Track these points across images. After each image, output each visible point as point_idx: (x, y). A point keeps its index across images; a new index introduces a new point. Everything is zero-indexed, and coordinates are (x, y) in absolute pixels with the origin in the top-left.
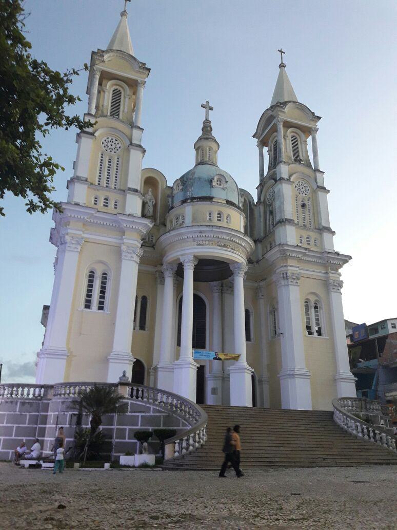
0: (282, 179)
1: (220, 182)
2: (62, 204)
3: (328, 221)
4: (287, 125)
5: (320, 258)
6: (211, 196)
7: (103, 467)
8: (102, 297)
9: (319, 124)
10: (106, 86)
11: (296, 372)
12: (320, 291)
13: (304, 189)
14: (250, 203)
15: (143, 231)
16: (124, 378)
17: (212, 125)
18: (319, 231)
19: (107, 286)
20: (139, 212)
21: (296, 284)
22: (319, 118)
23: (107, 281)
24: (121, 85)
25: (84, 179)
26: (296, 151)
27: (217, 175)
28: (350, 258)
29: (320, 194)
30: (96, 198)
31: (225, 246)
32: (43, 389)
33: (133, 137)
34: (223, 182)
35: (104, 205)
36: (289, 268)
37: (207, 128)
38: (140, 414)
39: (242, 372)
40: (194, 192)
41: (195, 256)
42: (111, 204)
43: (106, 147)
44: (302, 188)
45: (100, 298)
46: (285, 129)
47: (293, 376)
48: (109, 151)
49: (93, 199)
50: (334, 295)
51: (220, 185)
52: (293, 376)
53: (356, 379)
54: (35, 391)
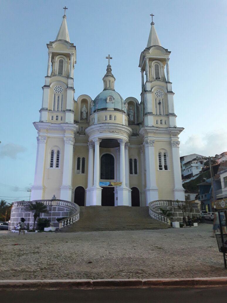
0: (147, 91)
3: (173, 110)
4: (151, 60)
5: (166, 131)
6: (106, 107)
7: (35, 232)
8: (58, 162)
9: (170, 56)
10: (55, 60)
11: (151, 188)
12: (167, 148)
13: (160, 95)
14: (137, 104)
15: (74, 129)
16: (54, 198)
17: (112, 68)
18: (167, 116)
20: (72, 122)
22: (170, 52)
24: (62, 57)
25: (46, 109)
26: (157, 73)
27: (109, 96)
28: (183, 129)
29: (169, 96)
31: (113, 132)
33: (68, 84)
34: (112, 99)
35: (56, 120)
36: (149, 138)
37: (109, 69)
38: (61, 212)
39: (122, 190)
40: (99, 106)
41: (99, 138)
42: (59, 118)
44: (159, 94)
45: (57, 162)
46: (154, 61)
47: (149, 190)
48: (58, 92)
49: (51, 117)
50: (174, 149)
51: (111, 101)
52: (149, 190)
53: (132, 190)
54: (174, 204)
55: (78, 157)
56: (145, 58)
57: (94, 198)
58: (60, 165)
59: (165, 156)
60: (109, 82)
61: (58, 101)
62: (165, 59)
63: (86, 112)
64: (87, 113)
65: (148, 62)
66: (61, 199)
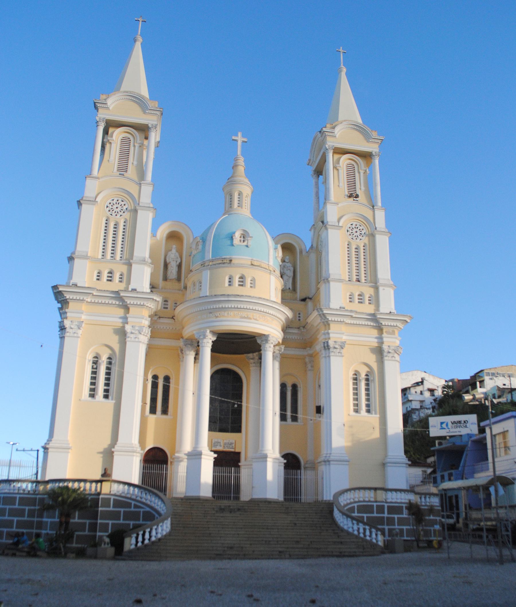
1: (244, 238)
2: (120, 292)
4: (341, 152)
11: (332, 458)
13: (358, 234)
20: (147, 288)
21: (340, 354)
42: (105, 276)
47: (327, 462)
48: (114, 214)
51: (244, 241)
52: (327, 462)
53: (285, 461)
56: (324, 148)
59: (367, 380)
60: (239, 195)
61: (115, 231)
62: (371, 153)
63: (178, 263)
64: (180, 266)
65: (331, 154)
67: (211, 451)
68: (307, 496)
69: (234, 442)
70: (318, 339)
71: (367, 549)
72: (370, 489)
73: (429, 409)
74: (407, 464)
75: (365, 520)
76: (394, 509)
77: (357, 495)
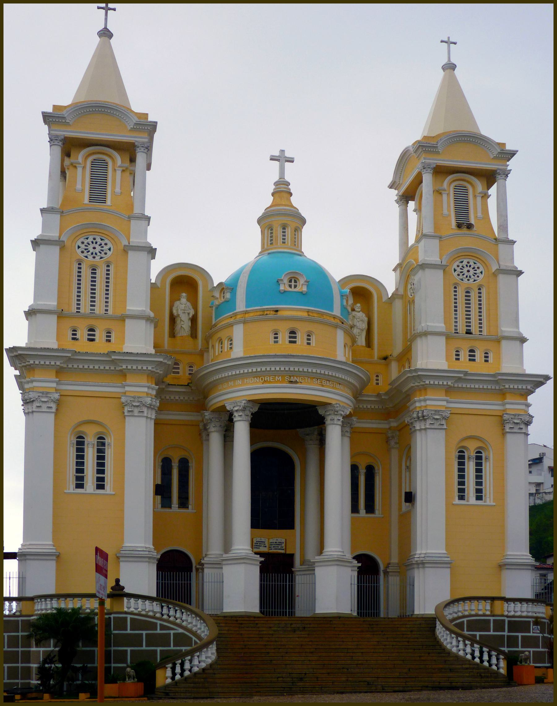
1: (295, 282)
9: (512, 164)
15: (158, 371)
19: (106, 455)
23: (106, 447)
30: (486, 353)
32: (14, 602)
43: (461, 274)
45: (97, 473)
51: (295, 286)
53: (360, 565)
54: (10, 606)
55: (163, 457)
57: (237, 588)
58: (108, 483)
63: (191, 316)
64: (194, 320)
66: (507, 597)
67: (256, 553)
68: (389, 608)
69: (284, 541)
70: (409, 407)
71: (483, 678)
72: (485, 599)
73: (549, 493)
74: (532, 565)
75: (478, 638)
76: (517, 625)
77: (467, 608)
